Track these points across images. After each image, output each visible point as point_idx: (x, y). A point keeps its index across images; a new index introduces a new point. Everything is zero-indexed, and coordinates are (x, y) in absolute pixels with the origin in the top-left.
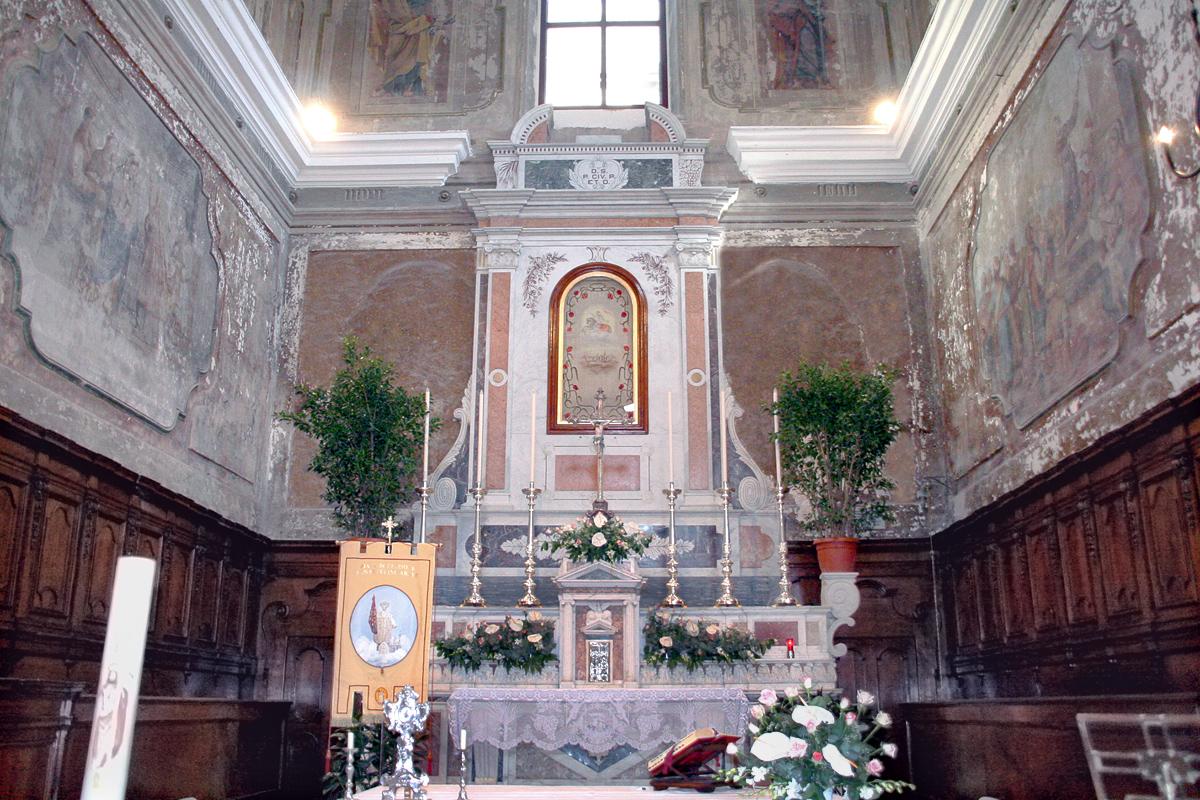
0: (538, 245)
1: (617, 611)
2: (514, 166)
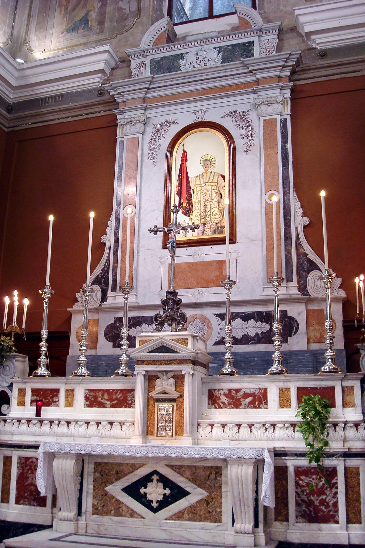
0: (157, 116)
1: (179, 379)
2: (142, 65)
